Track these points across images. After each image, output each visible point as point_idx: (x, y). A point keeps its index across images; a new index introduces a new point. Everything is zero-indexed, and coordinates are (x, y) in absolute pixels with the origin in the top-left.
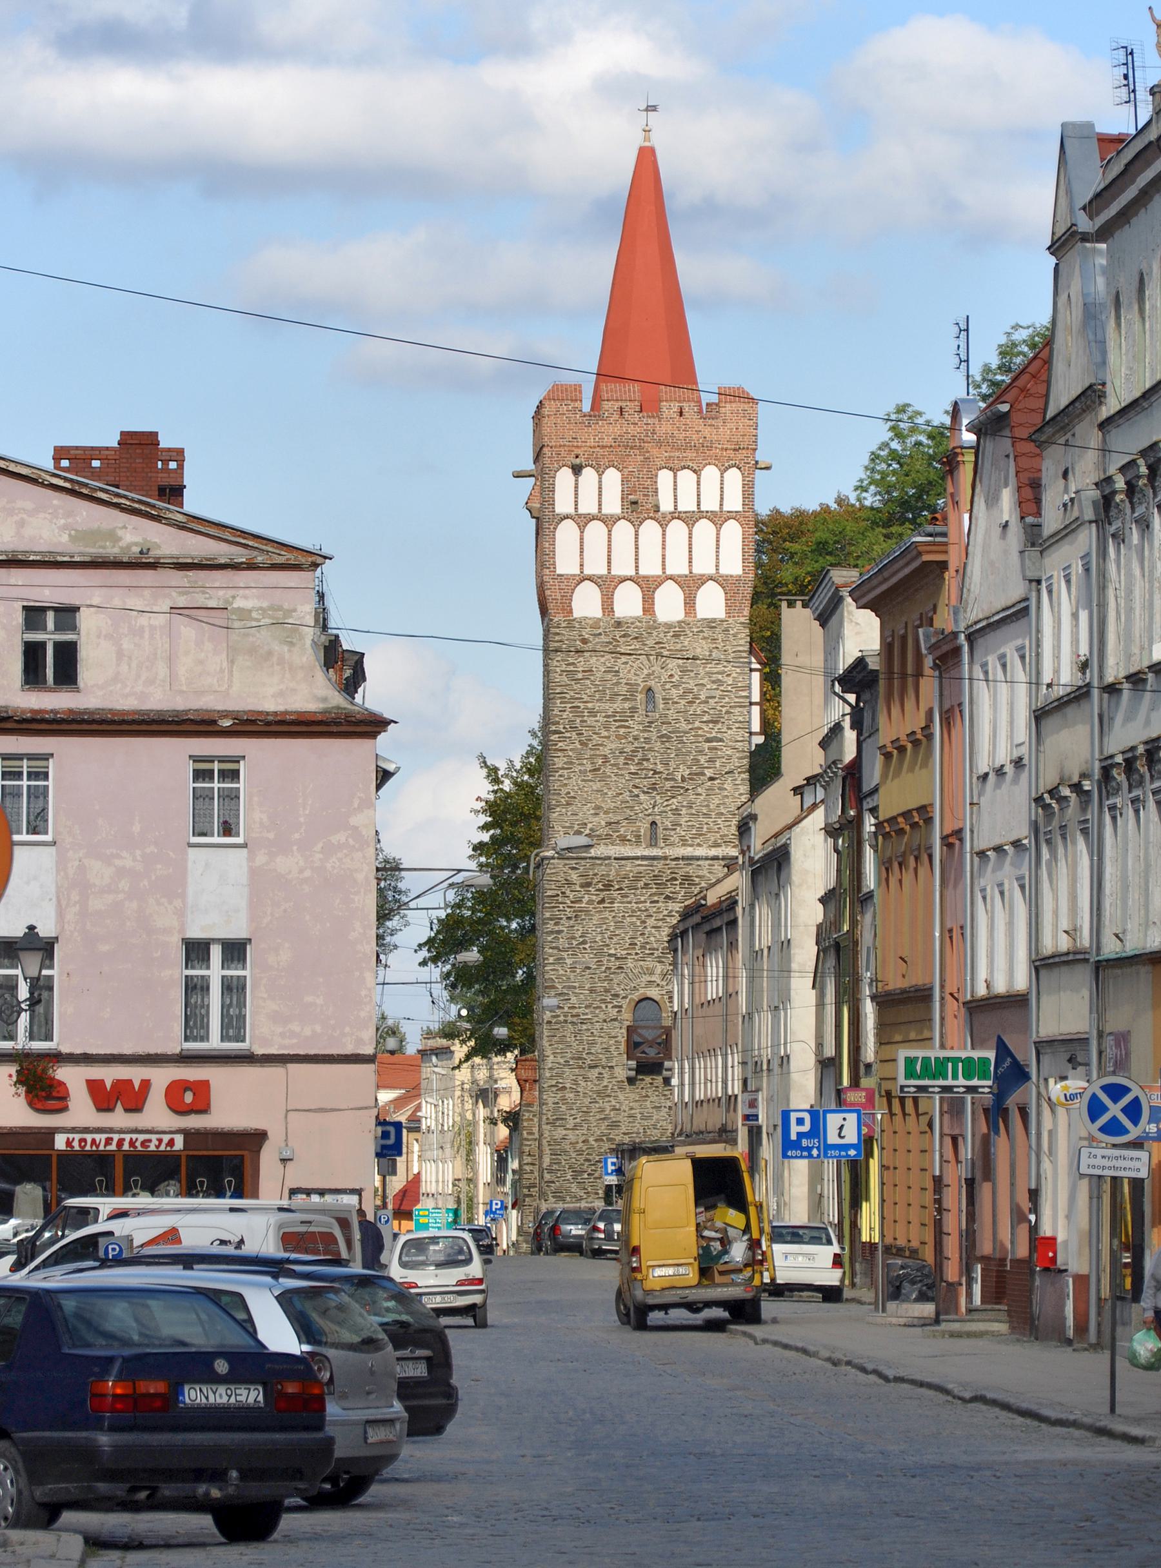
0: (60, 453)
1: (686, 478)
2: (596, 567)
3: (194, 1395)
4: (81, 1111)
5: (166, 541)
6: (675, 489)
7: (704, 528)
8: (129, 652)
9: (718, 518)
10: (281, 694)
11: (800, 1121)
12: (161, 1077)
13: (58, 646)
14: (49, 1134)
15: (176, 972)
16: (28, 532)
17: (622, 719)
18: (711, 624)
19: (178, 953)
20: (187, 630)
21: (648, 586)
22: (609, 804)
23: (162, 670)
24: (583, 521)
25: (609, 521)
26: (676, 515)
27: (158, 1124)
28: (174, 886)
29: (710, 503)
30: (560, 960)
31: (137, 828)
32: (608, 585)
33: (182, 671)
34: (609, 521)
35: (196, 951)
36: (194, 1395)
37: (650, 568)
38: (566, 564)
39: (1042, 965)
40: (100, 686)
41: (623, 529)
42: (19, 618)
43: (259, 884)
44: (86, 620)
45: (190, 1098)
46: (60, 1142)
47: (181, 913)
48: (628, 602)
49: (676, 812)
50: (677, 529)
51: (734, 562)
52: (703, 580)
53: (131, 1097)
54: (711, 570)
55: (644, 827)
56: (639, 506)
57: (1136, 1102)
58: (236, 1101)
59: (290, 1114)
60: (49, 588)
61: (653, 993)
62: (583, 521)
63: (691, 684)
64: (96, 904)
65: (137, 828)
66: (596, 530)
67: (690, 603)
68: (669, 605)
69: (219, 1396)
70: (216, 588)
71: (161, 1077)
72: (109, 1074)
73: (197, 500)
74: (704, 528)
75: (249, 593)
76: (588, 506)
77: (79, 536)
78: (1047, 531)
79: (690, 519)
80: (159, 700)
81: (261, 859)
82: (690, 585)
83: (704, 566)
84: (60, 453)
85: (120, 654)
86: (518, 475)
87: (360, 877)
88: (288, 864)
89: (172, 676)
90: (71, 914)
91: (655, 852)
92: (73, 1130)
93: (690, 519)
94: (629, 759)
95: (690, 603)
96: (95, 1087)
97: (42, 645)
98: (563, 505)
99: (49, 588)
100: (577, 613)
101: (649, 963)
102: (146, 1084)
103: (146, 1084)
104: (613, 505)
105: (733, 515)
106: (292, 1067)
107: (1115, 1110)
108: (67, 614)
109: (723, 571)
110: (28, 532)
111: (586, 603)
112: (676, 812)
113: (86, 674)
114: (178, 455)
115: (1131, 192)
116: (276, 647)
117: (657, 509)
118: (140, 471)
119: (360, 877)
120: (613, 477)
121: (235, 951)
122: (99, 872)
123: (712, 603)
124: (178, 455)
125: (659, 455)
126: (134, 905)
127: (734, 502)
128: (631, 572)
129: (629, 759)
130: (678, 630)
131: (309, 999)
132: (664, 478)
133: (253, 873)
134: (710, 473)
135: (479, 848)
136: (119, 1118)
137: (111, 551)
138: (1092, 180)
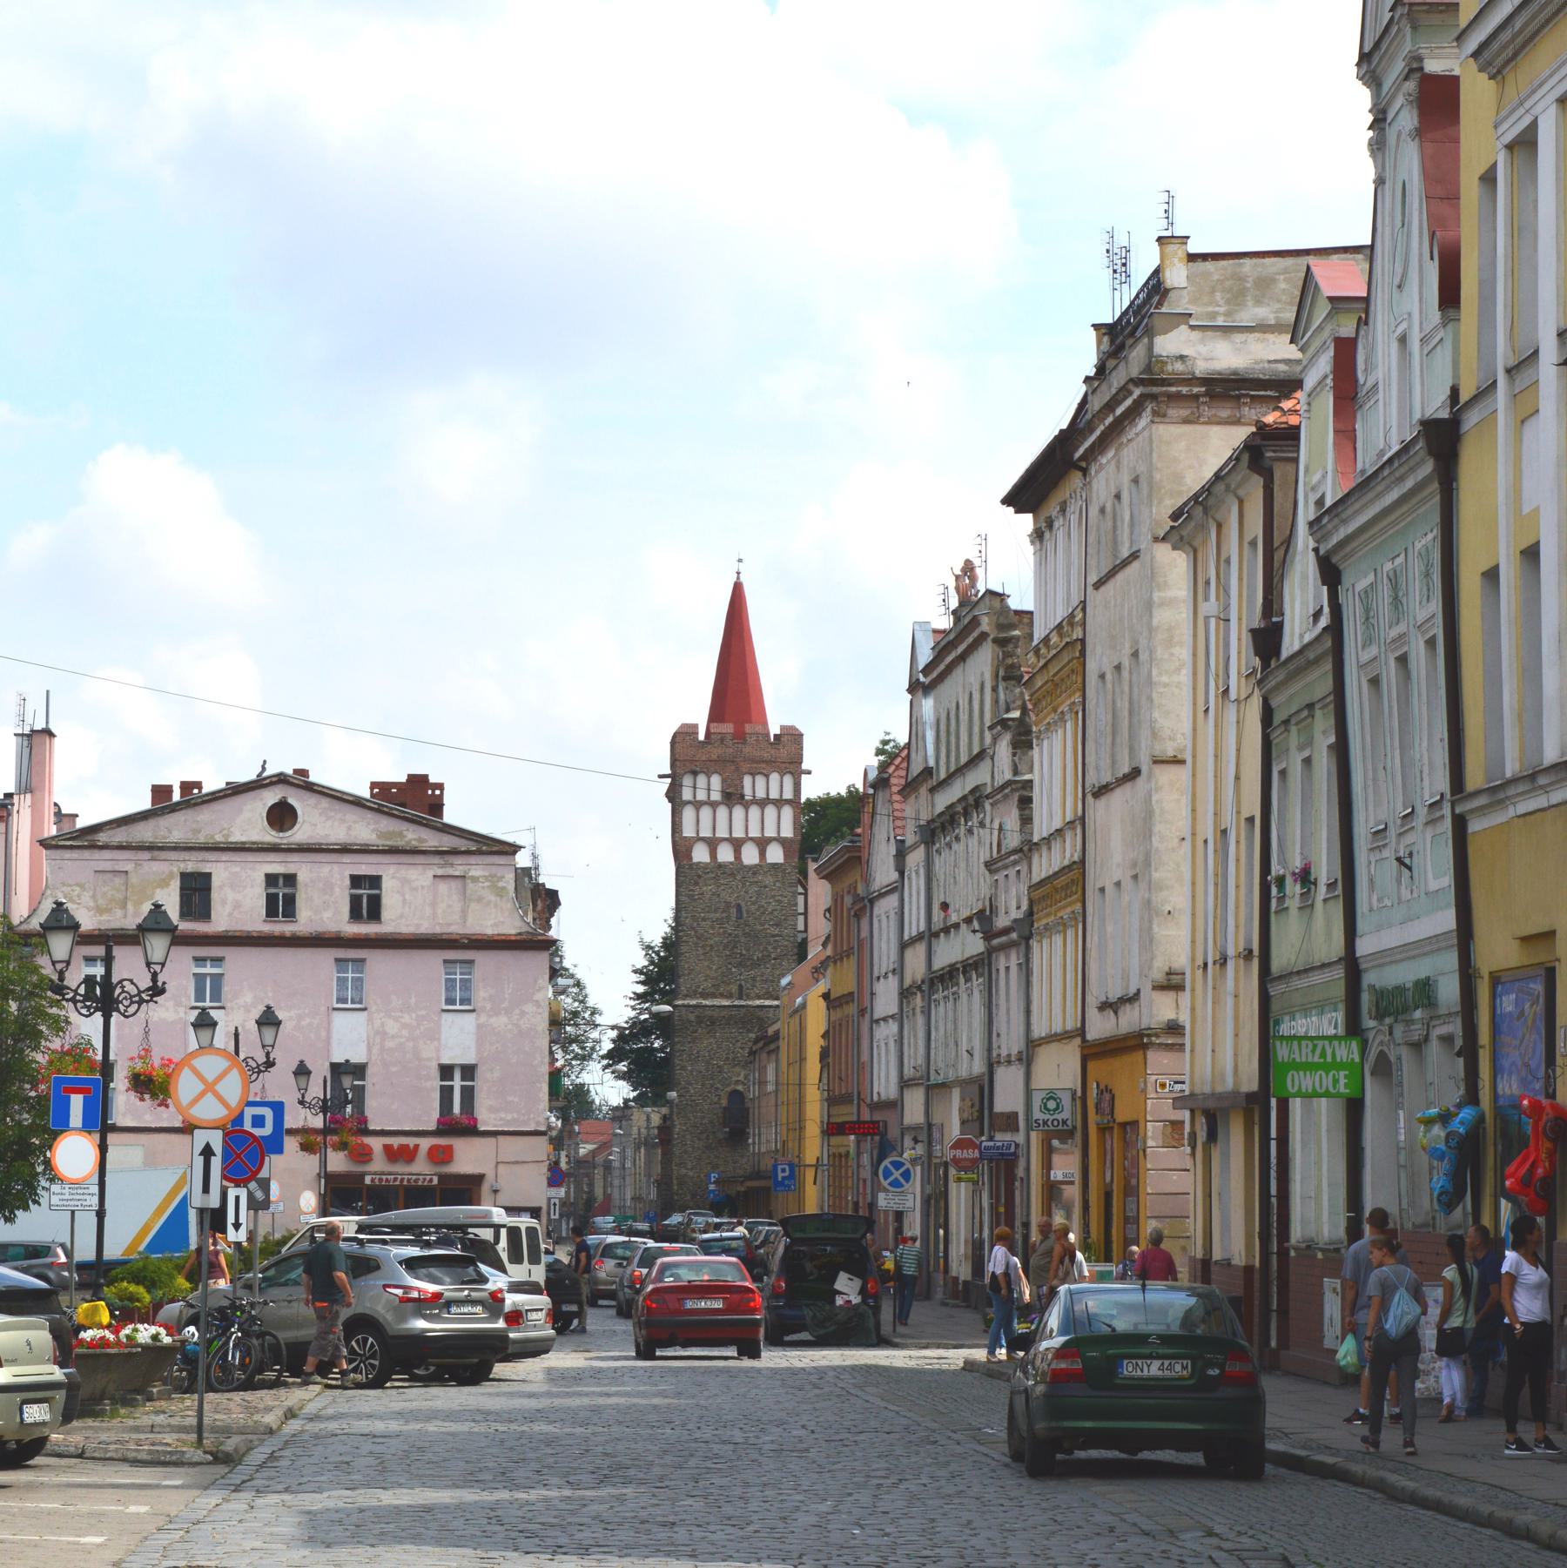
0: (373, 785)
1: (760, 780)
2: (706, 832)
3: (1129, 1369)
4: (378, 1164)
5: (432, 840)
6: (754, 786)
7: (770, 811)
8: (412, 900)
9: (779, 803)
10: (495, 925)
11: (783, 1171)
12: (425, 1144)
13: (369, 896)
14: (362, 1175)
15: (436, 1083)
16: (353, 833)
17: (721, 922)
18: (774, 866)
19: (436, 1073)
20: (443, 887)
21: (737, 844)
22: (713, 974)
23: (428, 911)
24: (698, 805)
25: (714, 805)
26: (755, 801)
27: (421, 1170)
28: (434, 1036)
29: (774, 795)
30: (683, 1068)
31: (413, 1000)
32: (713, 844)
33: (439, 911)
34: (714, 805)
35: (446, 1071)
36: (1129, 1369)
37: (738, 833)
38: (688, 831)
39: (904, 1084)
40: (398, 915)
41: (722, 812)
42: (348, 882)
43: (482, 1033)
44: (387, 884)
45: (441, 1156)
46: (368, 1180)
47: (438, 1050)
48: (725, 854)
49: (754, 979)
50: (754, 812)
51: (787, 832)
52: (770, 840)
53: (407, 1154)
54: (774, 835)
55: (734, 989)
56: (732, 797)
57: (908, 1171)
58: (468, 1157)
59: (501, 1168)
60: (365, 866)
61: (740, 1088)
62: (698, 805)
63: (763, 902)
64: (390, 1044)
65: (413, 1000)
66: (706, 812)
67: (762, 854)
68: (750, 856)
69: (1154, 1369)
70: (459, 866)
71: (425, 1144)
72: (396, 1142)
73: (450, 816)
74: (770, 811)
75: (477, 868)
76: (701, 796)
77: (381, 835)
78: (908, 844)
79: (763, 803)
80: (425, 927)
81: (483, 1019)
82: (762, 844)
83: (770, 832)
84: (373, 785)
85: (404, 901)
86: (661, 777)
87: (540, 1029)
88: (500, 1022)
89: (434, 914)
90: (375, 1051)
91: (742, 1003)
92: (376, 1173)
93: (763, 803)
94: (726, 947)
95: (762, 854)
96: (387, 1148)
97: (360, 896)
98: (687, 794)
99: (365, 866)
100: (695, 860)
101: (737, 1069)
102: (417, 1147)
103: (417, 1147)
104: (716, 796)
105: (788, 802)
106: (501, 1138)
107: (897, 1174)
108: (375, 881)
109: (783, 834)
110: (353, 833)
111: (700, 854)
112: (754, 979)
113: (386, 914)
114: (440, 786)
115: (942, 667)
116: (493, 898)
117: (742, 796)
118: (415, 799)
119: (540, 1029)
120: (716, 781)
121: (469, 1071)
122: (392, 1027)
123: (775, 855)
124: (440, 786)
125: (745, 767)
126: (411, 1044)
127: (788, 795)
128: (727, 836)
129: (726, 947)
130: (754, 870)
131: (510, 1098)
132: (747, 780)
133: (479, 1027)
134: (775, 777)
135: (638, 996)
136: (400, 1168)
137: (400, 843)
138: (925, 657)
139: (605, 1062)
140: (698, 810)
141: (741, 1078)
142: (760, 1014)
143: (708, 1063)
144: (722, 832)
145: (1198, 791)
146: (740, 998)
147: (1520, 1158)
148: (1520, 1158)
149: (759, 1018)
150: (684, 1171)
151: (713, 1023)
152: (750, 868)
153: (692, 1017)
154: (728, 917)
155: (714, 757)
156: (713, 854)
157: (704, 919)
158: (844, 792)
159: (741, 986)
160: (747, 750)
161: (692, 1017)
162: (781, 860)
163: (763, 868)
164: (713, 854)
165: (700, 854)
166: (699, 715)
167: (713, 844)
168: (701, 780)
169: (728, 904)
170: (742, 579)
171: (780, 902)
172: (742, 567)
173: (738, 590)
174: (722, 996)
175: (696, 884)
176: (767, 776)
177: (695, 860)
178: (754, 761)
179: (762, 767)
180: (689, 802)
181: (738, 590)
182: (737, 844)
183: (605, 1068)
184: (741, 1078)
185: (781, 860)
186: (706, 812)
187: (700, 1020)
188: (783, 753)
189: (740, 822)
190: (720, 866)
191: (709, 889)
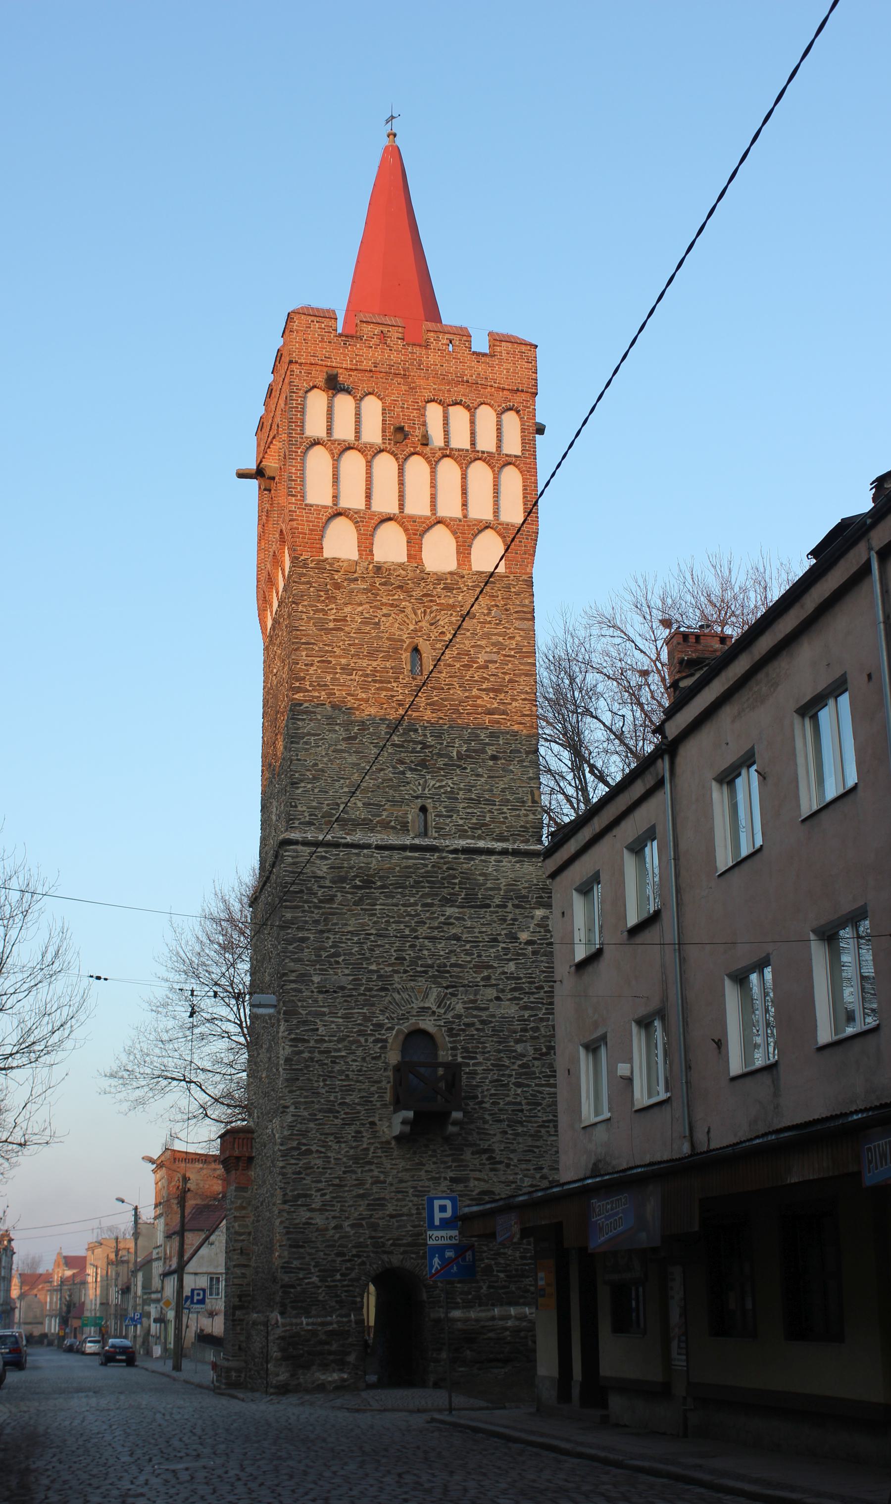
1: (459, 416)
32: (368, 524)
34: (370, 453)
37: (417, 506)
48: (390, 546)
56: (403, 438)
67: (464, 551)
79: (466, 458)
82: (465, 532)
83: (480, 510)
93: (466, 458)
100: (329, 552)
104: (373, 433)
112: (452, 796)
117: (425, 441)
120: (372, 407)
130: (449, 582)
132: (434, 413)
140: (359, 401)
141: (431, 1003)
143: (357, 967)
145: (833, 806)
147: (483, 1404)
148: (483, 1404)
151: (368, 883)
152: (439, 578)
153: (322, 868)
154: (398, 670)
155: (367, 365)
156: (366, 545)
157: (347, 670)
160: (432, 358)
161: (322, 868)
164: (366, 545)
165: (340, 543)
166: (335, 296)
167: (368, 524)
169: (395, 642)
170: (398, 141)
171: (500, 646)
172: (397, 126)
174: (385, 826)
177: (329, 552)
179: (466, 393)
182: (416, 531)
186: (353, 463)
188: (503, 373)
189: (419, 485)
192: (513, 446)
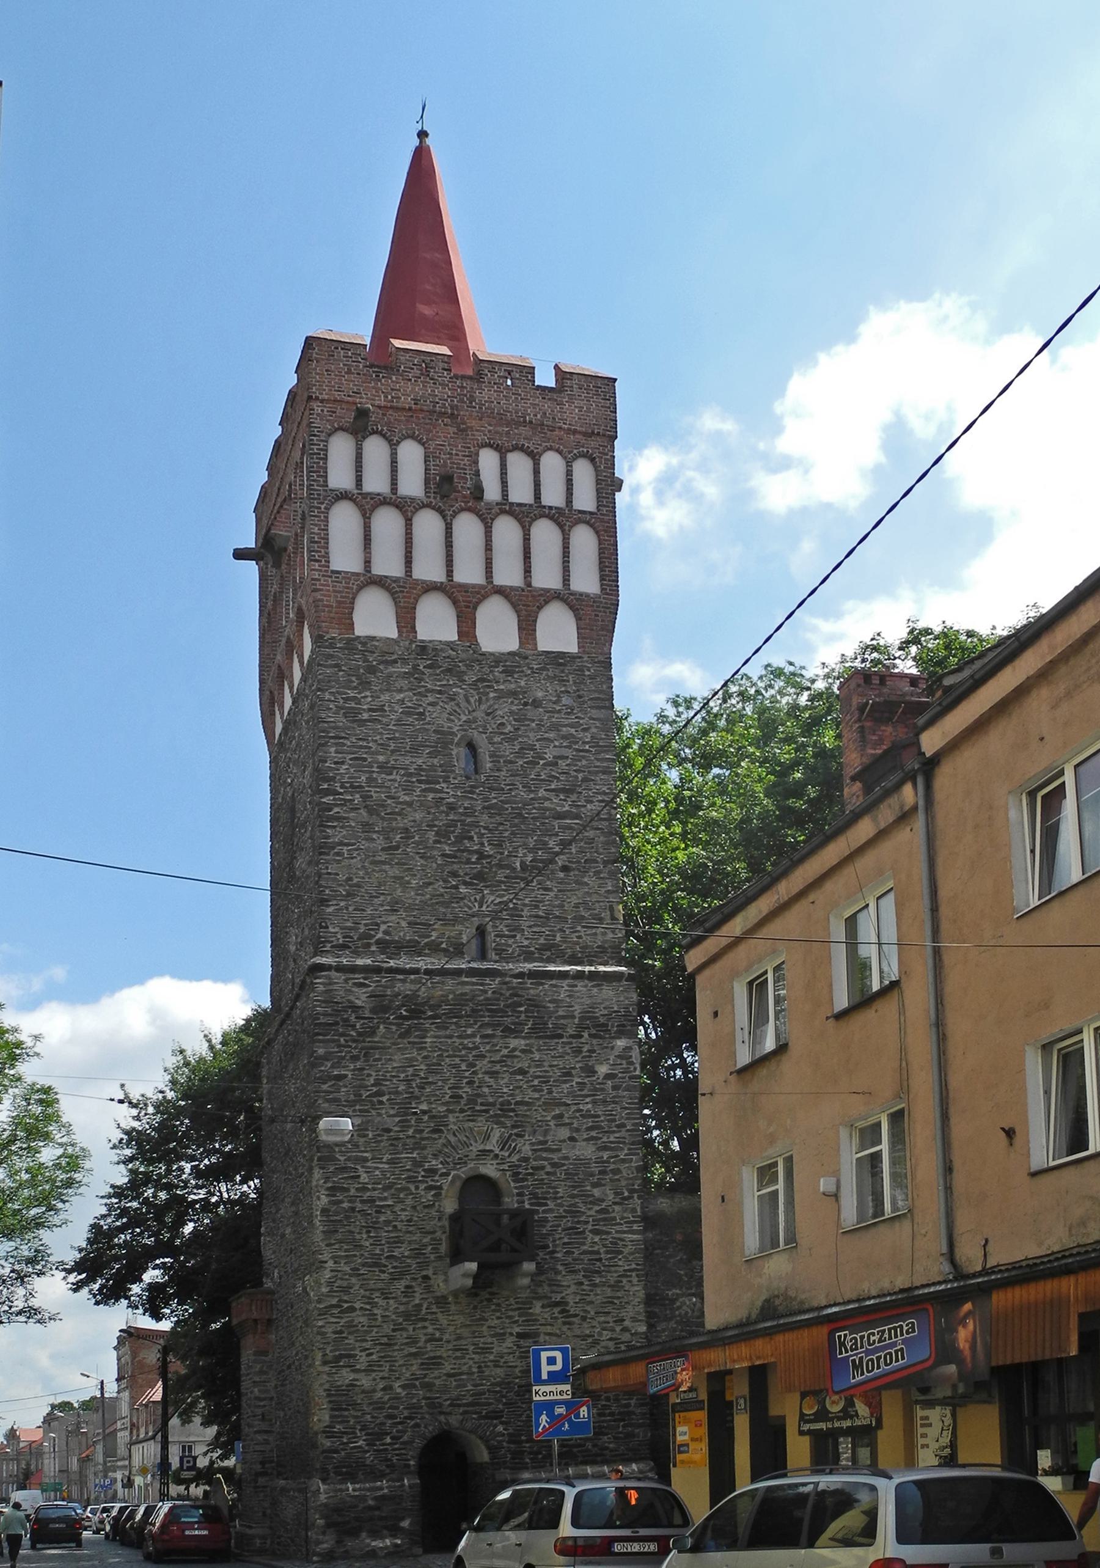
3: (51, 1526)
18: (557, 659)
24: (367, 505)
25: (407, 508)
34: (407, 508)
36: (51, 1526)
37: (468, 573)
41: (428, 524)
48: (436, 623)
49: (515, 914)
52: (548, 597)
55: (467, 934)
56: (451, 491)
66: (387, 524)
67: (527, 628)
93: (525, 516)
94: (442, 835)
100: (360, 630)
101: (481, 1124)
104: (412, 484)
117: (478, 492)
120: (411, 454)
129: (442, 835)
130: (508, 663)
139: (73, 1278)
141: (492, 1145)
142: (533, 990)
143: (404, 1111)
144: (429, 569)
146: (483, 956)
149: (534, 1004)
150: (346, 1376)
151: (416, 1013)
152: (498, 659)
154: (448, 768)
155: (406, 401)
156: (406, 619)
157: (384, 768)
158: (822, 357)
159: (481, 932)
161: (361, 998)
162: (573, 648)
163: (525, 660)
164: (406, 619)
167: (405, 594)
168: (375, 449)
169: (444, 740)
171: (571, 739)
173: (421, 171)
174: (434, 948)
175: (365, 685)
176: (535, 458)
177: (360, 630)
178: (501, 419)
180: (343, 496)
181: (421, 171)
182: (466, 602)
183: (77, 1287)
184: (492, 1145)
185: (573, 648)
186: (387, 523)
187: (381, 1006)
188: (572, 413)
190: (423, 649)
191: (396, 699)
192: (585, 499)
